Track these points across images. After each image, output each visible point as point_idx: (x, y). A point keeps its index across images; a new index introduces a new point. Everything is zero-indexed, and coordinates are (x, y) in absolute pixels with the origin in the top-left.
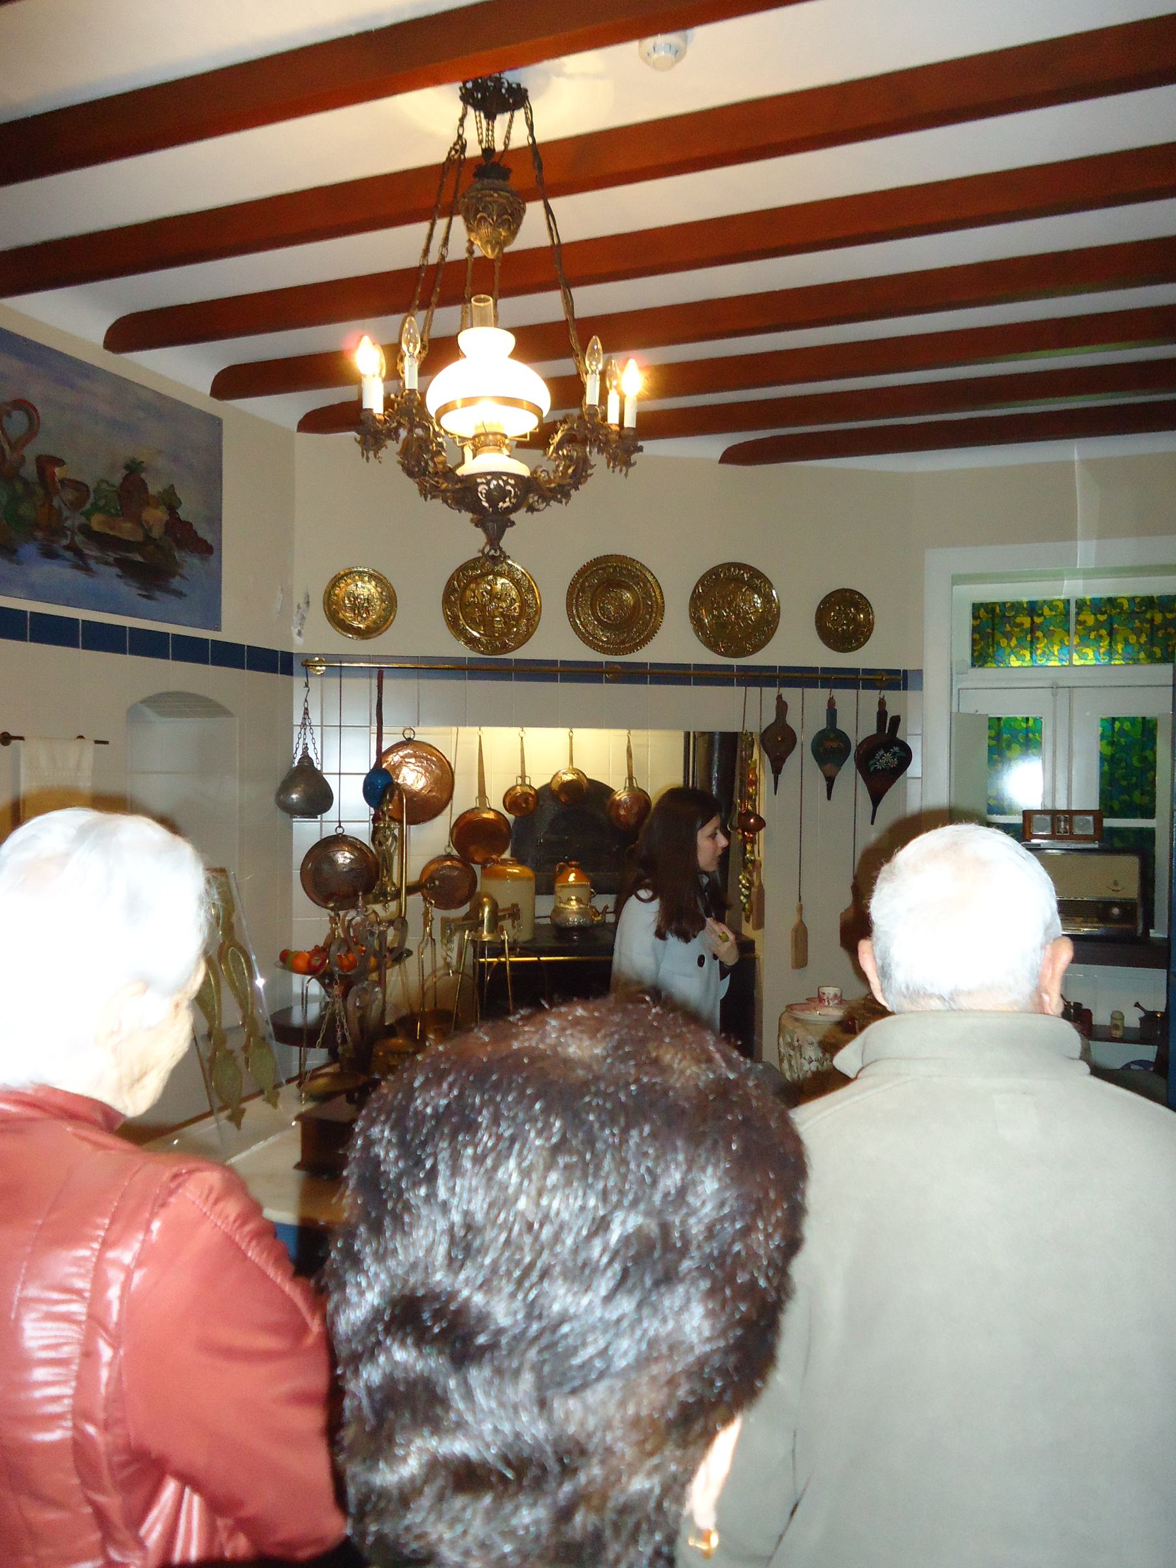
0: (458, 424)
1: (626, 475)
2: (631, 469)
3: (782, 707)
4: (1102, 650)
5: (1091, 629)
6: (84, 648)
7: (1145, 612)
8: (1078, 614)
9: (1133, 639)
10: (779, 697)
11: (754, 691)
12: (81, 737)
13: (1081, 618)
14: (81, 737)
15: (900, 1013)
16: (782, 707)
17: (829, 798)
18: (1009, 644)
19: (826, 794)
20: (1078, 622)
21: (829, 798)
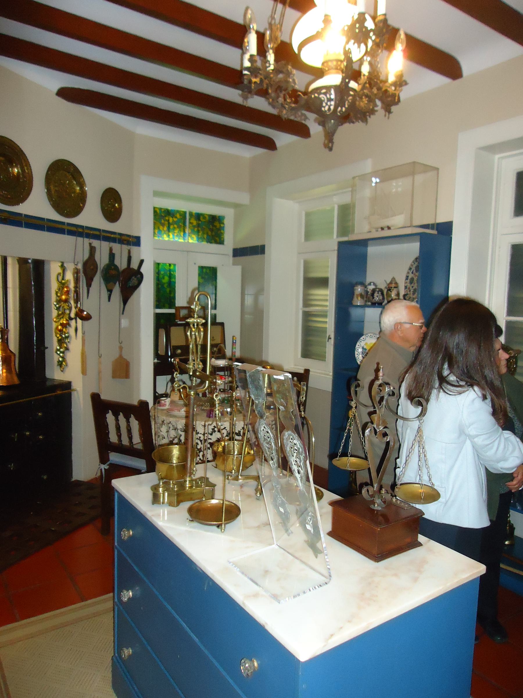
0: (311, 57)
1: (388, 118)
2: (391, 115)
3: (92, 250)
4: (175, 234)
5: (194, 227)
6: (68, 235)
7: (165, 216)
8: (190, 220)
9: (210, 233)
10: (111, 249)
11: (80, 239)
12: (341, 628)
13: (191, 221)
14: (341, 628)
15: (259, 527)
16: (92, 250)
17: (109, 300)
18: (163, 229)
19: (107, 300)
20: (190, 223)
21: (109, 300)
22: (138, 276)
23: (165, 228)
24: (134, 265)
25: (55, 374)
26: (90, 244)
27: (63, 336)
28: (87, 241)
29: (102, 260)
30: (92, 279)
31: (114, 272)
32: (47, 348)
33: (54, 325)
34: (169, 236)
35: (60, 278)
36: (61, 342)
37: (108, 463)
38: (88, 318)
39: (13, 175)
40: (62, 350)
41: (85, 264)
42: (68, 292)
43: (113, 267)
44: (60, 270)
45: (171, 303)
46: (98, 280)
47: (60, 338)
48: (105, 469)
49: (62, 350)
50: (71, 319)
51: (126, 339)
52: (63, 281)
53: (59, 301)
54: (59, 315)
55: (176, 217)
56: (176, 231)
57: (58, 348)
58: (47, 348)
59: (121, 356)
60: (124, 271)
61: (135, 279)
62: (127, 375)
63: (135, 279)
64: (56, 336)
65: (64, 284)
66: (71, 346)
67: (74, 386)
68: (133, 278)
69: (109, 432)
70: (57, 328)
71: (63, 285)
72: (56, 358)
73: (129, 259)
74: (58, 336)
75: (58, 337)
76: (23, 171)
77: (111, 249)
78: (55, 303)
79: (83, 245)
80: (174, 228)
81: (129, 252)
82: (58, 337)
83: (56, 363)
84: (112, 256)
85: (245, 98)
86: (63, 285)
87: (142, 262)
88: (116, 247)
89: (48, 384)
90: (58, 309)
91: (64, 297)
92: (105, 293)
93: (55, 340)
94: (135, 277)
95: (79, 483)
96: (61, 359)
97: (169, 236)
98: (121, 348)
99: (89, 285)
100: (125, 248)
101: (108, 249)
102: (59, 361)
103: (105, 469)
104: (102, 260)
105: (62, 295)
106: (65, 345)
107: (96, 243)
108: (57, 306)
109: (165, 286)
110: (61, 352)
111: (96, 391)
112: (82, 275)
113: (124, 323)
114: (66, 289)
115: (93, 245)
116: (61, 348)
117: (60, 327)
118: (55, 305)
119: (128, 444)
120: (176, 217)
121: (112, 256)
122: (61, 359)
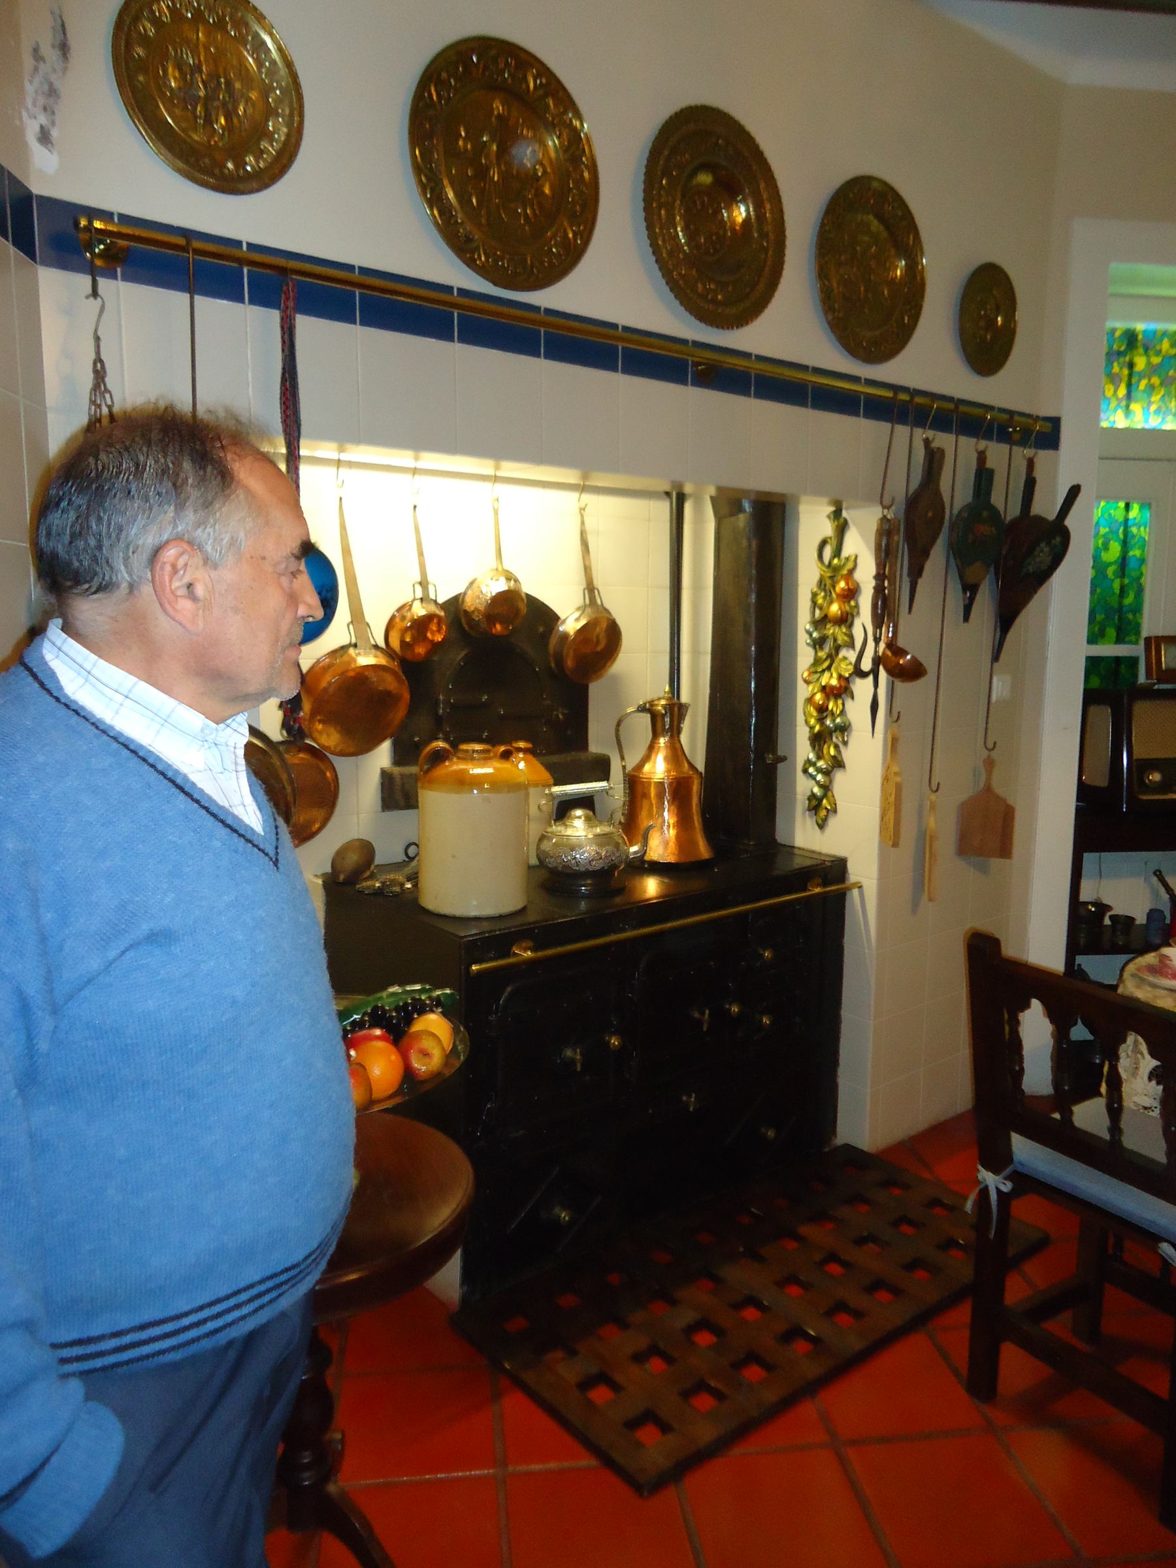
3: (934, 459)
4: (1153, 407)
10: (982, 457)
11: (902, 431)
16: (934, 459)
17: (966, 618)
21: (966, 618)
22: (1055, 537)
23: (1122, 391)
24: (1046, 506)
25: (806, 837)
26: (927, 442)
27: (828, 722)
28: (920, 434)
29: (956, 490)
30: (925, 553)
31: (986, 530)
32: (783, 759)
33: (803, 691)
34: (1127, 411)
35: (828, 552)
36: (818, 740)
37: (1008, 1171)
38: (913, 672)
39: (733, 230)
40: (821, 764)
41: (912, 503)
42: (851, 593)
43: (985, 514)
44: (827, 529)
45: (1125, 628)
46: (937, 560)
47: (817, 728)
48: (998, 1191)
49: (821, 764)
50: (859, 673)
51: (1000, 739)
52: (836, 561)
53: (820, 623)
54: (817, 661)
55: (1158, 353)
56: (1156, 398)
57: (812, 756)
58: (783, 759)
59: (988, 789)
60: (1015, 522)
61: (1046, 550)
62: (1005, 849)
63: (1046, 550)
64: (807, 722)
65: (835, 570)
66: (847, 755)
67: (855, 872)
68: (1043, 545)
69: (1022, 1070)
70: (810, 700)
71: (836, 572)
72: (804, 787)
73: (1030, 484)
74: (812, 721)
75: (812, 728)
76: (760, 216)
77: (982, 457)
78: (808, 627)
79: (907, 441)
80: (1151, 388)
81: (1031, 464)
82: (812, 728)
83: (801, 802)
84: (984, 477)
85: (497, 468)
86: (836, 572)
87: (1074, 492)
88: (997, 453)
89: (782, 867)
90: (818, 644)
91: (835, 608)
92: (955, 598)
93: (802, 736)
94: (1049, 543)
95: (853, 1157)
96: (816, 790)
97: (1127, 411)
98: (990, 764)
99: (916, 572)
100: (1021, 454)
101: (975, 456)
102: (813, 796)
103: (998, 1191)
104: (956, 490)
105: (831, 602)
106: (832, 752)
107: (944, 440)
108: (815, 635)
109: (1110, 571)
110: (819, 770)
111: (986, 925)
112: (899, 538)
113: (1000, 687)
114: (842, 584)
115: (935, 445)
116: (819, 757)
117: (819, 697)
118: (810, 634)
119: (1107, 1137)
120: (1158, 353)
121: (984, 477)
122: (816, 790)
